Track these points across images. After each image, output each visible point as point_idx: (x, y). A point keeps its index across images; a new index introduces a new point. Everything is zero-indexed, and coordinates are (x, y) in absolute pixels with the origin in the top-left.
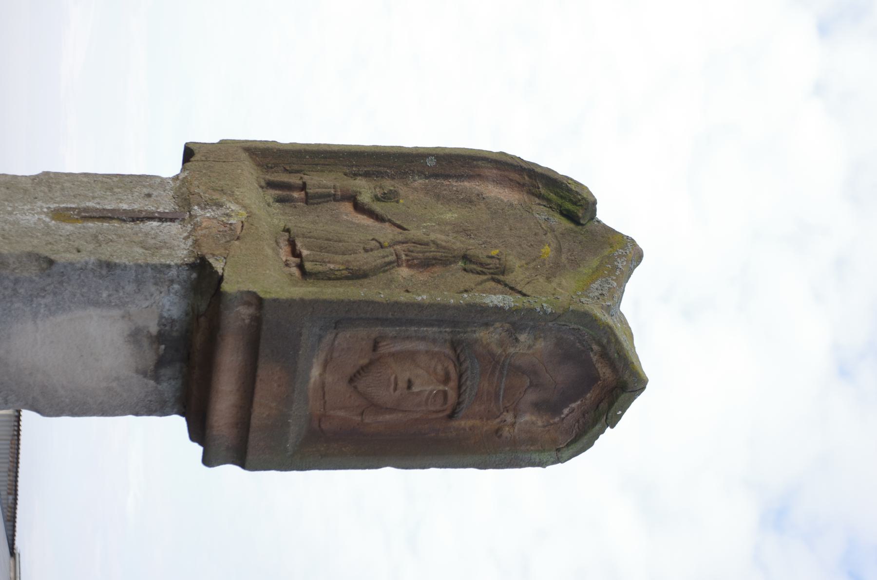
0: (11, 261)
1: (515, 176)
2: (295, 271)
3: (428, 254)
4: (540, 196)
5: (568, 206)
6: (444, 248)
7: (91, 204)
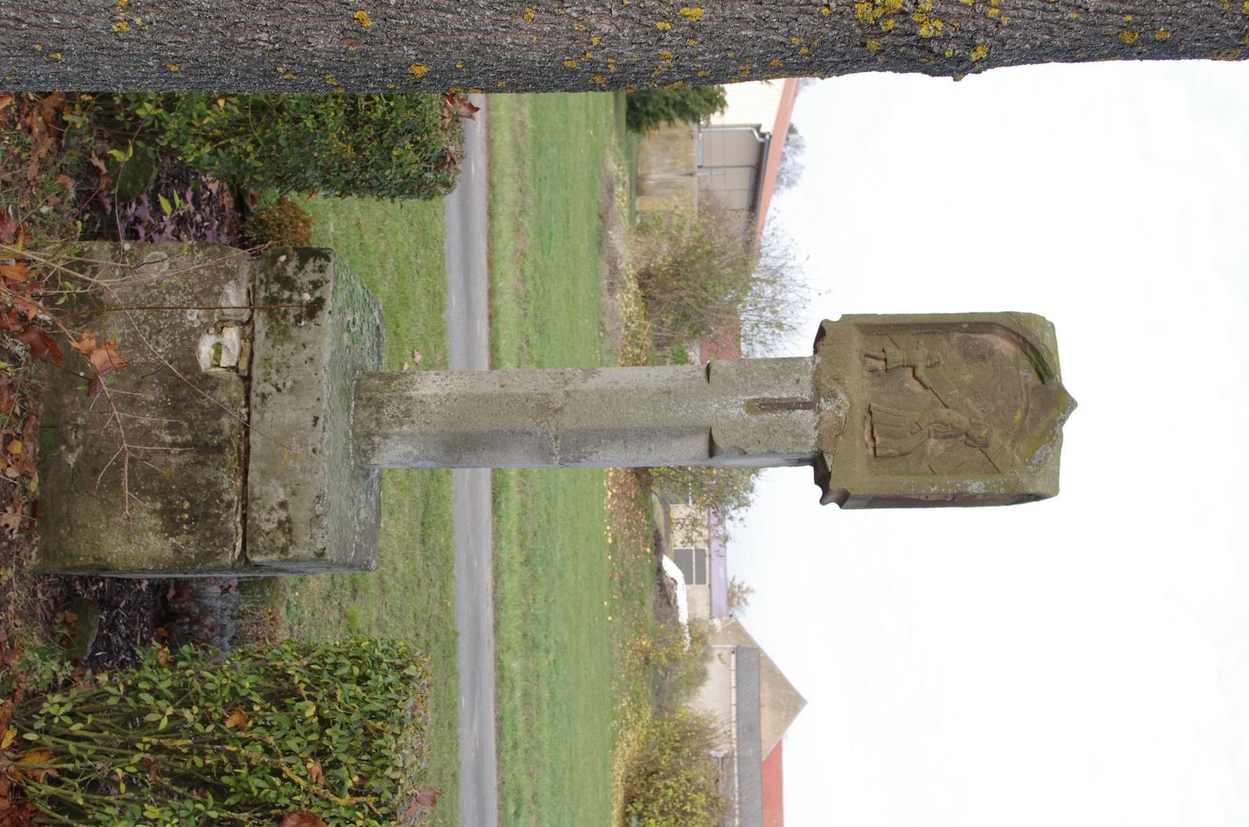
1: (1015, 338)
2: (871, 451)
7: (767, 395)
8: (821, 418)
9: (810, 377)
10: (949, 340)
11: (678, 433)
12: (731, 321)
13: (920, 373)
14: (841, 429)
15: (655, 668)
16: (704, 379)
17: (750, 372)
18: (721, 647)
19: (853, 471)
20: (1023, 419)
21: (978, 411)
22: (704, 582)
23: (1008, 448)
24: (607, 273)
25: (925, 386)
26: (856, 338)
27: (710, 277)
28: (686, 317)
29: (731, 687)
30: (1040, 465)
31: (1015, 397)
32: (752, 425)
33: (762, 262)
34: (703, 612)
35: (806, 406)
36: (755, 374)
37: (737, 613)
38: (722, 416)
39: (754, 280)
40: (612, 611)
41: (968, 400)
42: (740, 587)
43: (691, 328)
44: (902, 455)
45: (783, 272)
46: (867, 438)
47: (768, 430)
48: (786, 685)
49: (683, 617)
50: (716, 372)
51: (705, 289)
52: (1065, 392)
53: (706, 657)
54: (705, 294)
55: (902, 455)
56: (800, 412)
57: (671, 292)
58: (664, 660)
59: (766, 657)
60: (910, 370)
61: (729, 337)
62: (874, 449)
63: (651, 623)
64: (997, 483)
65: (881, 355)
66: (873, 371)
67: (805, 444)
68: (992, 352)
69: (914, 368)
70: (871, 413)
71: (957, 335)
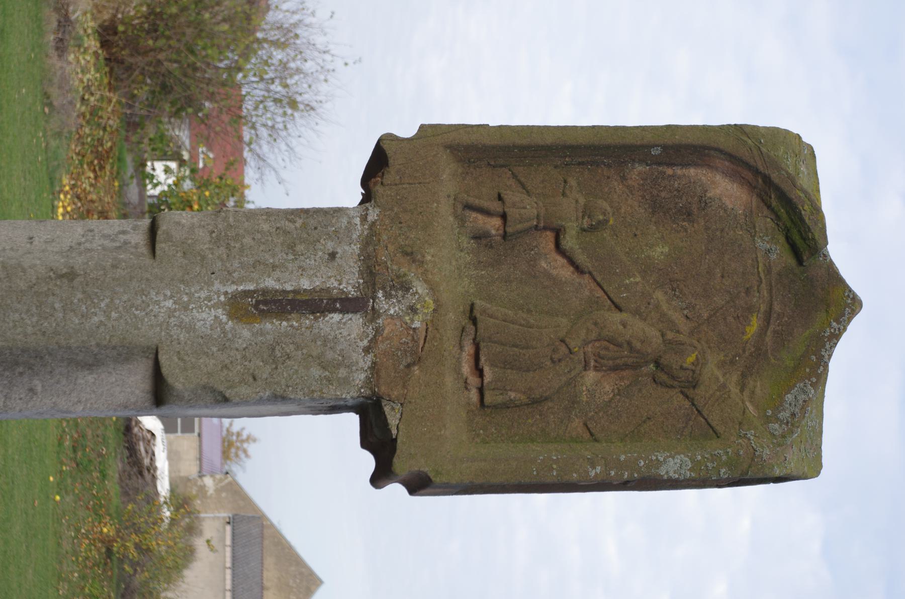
0: (186, 395)
1: (749, 175)
2: (474, 395)
3: (618, 361)
4: (769, 207)
5: (796, 237)
6: (638, 352)
7: (270, 283)
8: (378, 331)
9: (356, 248)
10: (623, 178)
11: (90, 359)
12: (227, 97)
13: (570, 242)
14: (418, 353)
15: (121, 561)
16: (144, 250)
17: (237, 238)
18: (213, 526)
19: (438, 414)
20: (763, 331)
21: (677, 317)
22: (192, 430)
23: (734, 390)
24: (55, 24)
25: (578, 269)
26: (448, 171)
27: (199, 36)
28: (165, 89)
29: (225, 568)
30: (792, 423)
31: (748, 291)
32: (240, 344)
33: (271, 16)
34: (189, 468)
35: (348, 305)
36: (247, 240)
37: (235, 468)
38: (180, 326)
39: (258, 41)
40: (61, 488)
41: (659, 295)
42: (239, 434)
43: (173, 104)
44: (535, 402)
45: (299, 31)
46: (466, 369)
47: (273, 354)
48: (297, 561)
49: (163, 487)
50: (169, 237)
51: (192, 52)
52: (841, 281)
53: (192, 530)
54: (192, 59)
55: (535, 402)
56: (336, 317)
57: (145, 53)
58: (133, 553)
59: (272, 526)
60: (550, 235)
61: (226, 118)
62: (481, 391)
63: (116, 501)
64: (714, 458)
65: (496, 206)
66: (480, 237)
67: (346, 381)
68: (704, 203)
69: (558, 233)
70: (474, 321)
71: (640, 168)
